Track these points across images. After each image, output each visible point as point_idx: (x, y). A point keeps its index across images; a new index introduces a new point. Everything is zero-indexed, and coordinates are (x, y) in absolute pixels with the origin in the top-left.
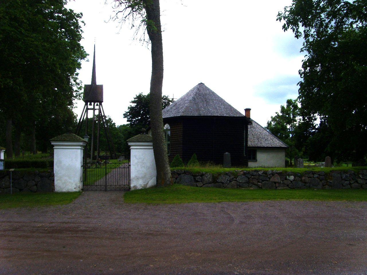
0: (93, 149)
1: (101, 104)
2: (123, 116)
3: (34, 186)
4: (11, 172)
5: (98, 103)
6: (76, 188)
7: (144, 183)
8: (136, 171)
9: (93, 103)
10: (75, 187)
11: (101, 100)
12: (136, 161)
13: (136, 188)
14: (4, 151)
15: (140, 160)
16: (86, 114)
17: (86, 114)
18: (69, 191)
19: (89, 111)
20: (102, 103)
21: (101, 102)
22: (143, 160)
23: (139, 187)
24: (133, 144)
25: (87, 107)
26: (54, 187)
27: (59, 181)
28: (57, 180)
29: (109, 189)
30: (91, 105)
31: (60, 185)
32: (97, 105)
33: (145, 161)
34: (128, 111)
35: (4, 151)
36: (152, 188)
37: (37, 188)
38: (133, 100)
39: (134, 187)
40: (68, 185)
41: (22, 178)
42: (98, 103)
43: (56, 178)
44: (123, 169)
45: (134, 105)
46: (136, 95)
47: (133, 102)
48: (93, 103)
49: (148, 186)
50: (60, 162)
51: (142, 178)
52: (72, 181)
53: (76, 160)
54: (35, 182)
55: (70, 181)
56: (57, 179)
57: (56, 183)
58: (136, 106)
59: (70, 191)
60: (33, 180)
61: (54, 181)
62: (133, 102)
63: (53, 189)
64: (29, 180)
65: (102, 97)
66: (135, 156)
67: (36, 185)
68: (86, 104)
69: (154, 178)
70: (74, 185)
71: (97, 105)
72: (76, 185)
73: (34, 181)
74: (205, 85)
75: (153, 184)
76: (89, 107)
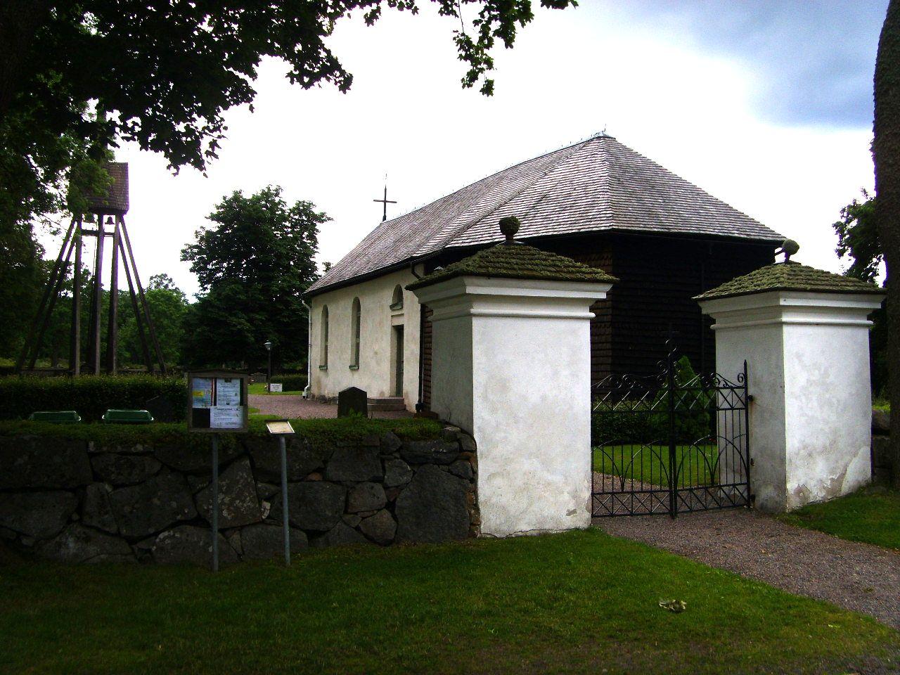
0: (95, 349)
1: (120, 219)
2: (179, 255)
3: (379, 510)
4: (283, 440)
5: (114, 217)
6: (574, 512)
7: (832, 472)
8: (803, 419)
9: (96, 217)
10: (572, 508)
11: (124, 208)
12: (802, 379)
13: (806, 498)
14: (595, 306)
15: (816, 375)
16: (74, 248)
17: (74, 248)
18: (547, 527)
19: (85, 239)
20: (125, 217)
21: (120, 211)
22: (826, 374)
23: (817, 494)
24: (815, 305)
25: (79, 225)
26: (478, 510)
27: (498, 481)
28: (492, 476)
29: (684, 508)
30: (90, 220)
31: (504, 500)
32: (110, 221)
33: (831, 378)
34: (195, 242)
35: (595, 306)
36: (859, 492)
37: (395, 517)
38: (215, 212)
39: (800, 491)
40: (539, 498)
41: (319, 470)
42: (114, 217)
43: (484, 468)
44: (729, 412)
45: (214, 226)
46: (224, 198)
47: (213, 217)
48: (96, 217)
49: (846, 488)
50: (504, 386)
51: (825, 451)
52: (557, 479)
53: (574, 375)
54: (386, 488)
55: (550, 477)
56: (492, 470)
57: (485, 488)
58: (222, 230)
59: (549, 526)
60: (379, 480)
61: (474, 480)
62: (213, 217)
63: (475, 523)
64: (358, 482)
65: (126, 199)
66: (799, 357)
67: (390, 506)
68: (77, 219)
69: (862, 450)
70: (566, 497)
71: (110, 221)
72: (574, 497)
73: (379, 487)
74: (619, 140)
75: (860, 479)
76: (86, 226)
